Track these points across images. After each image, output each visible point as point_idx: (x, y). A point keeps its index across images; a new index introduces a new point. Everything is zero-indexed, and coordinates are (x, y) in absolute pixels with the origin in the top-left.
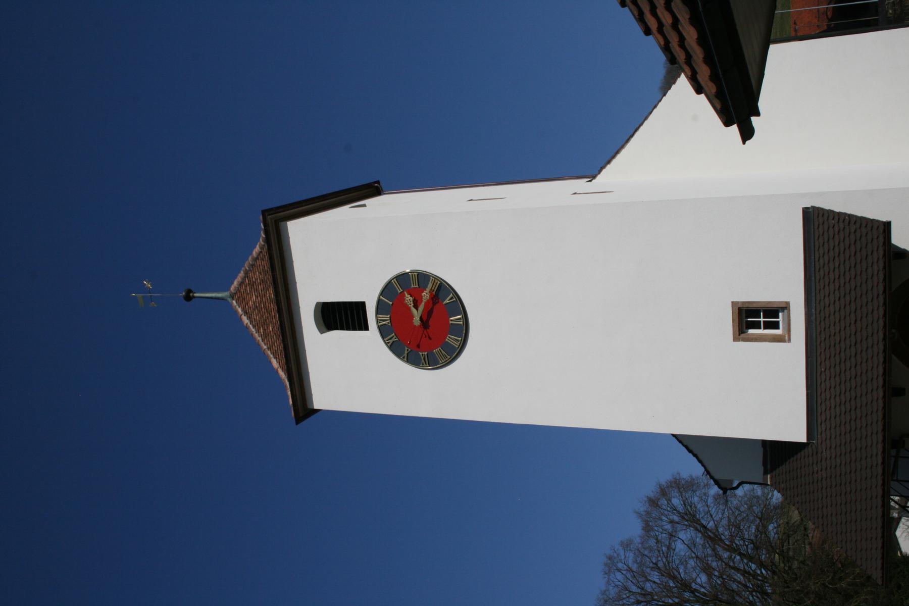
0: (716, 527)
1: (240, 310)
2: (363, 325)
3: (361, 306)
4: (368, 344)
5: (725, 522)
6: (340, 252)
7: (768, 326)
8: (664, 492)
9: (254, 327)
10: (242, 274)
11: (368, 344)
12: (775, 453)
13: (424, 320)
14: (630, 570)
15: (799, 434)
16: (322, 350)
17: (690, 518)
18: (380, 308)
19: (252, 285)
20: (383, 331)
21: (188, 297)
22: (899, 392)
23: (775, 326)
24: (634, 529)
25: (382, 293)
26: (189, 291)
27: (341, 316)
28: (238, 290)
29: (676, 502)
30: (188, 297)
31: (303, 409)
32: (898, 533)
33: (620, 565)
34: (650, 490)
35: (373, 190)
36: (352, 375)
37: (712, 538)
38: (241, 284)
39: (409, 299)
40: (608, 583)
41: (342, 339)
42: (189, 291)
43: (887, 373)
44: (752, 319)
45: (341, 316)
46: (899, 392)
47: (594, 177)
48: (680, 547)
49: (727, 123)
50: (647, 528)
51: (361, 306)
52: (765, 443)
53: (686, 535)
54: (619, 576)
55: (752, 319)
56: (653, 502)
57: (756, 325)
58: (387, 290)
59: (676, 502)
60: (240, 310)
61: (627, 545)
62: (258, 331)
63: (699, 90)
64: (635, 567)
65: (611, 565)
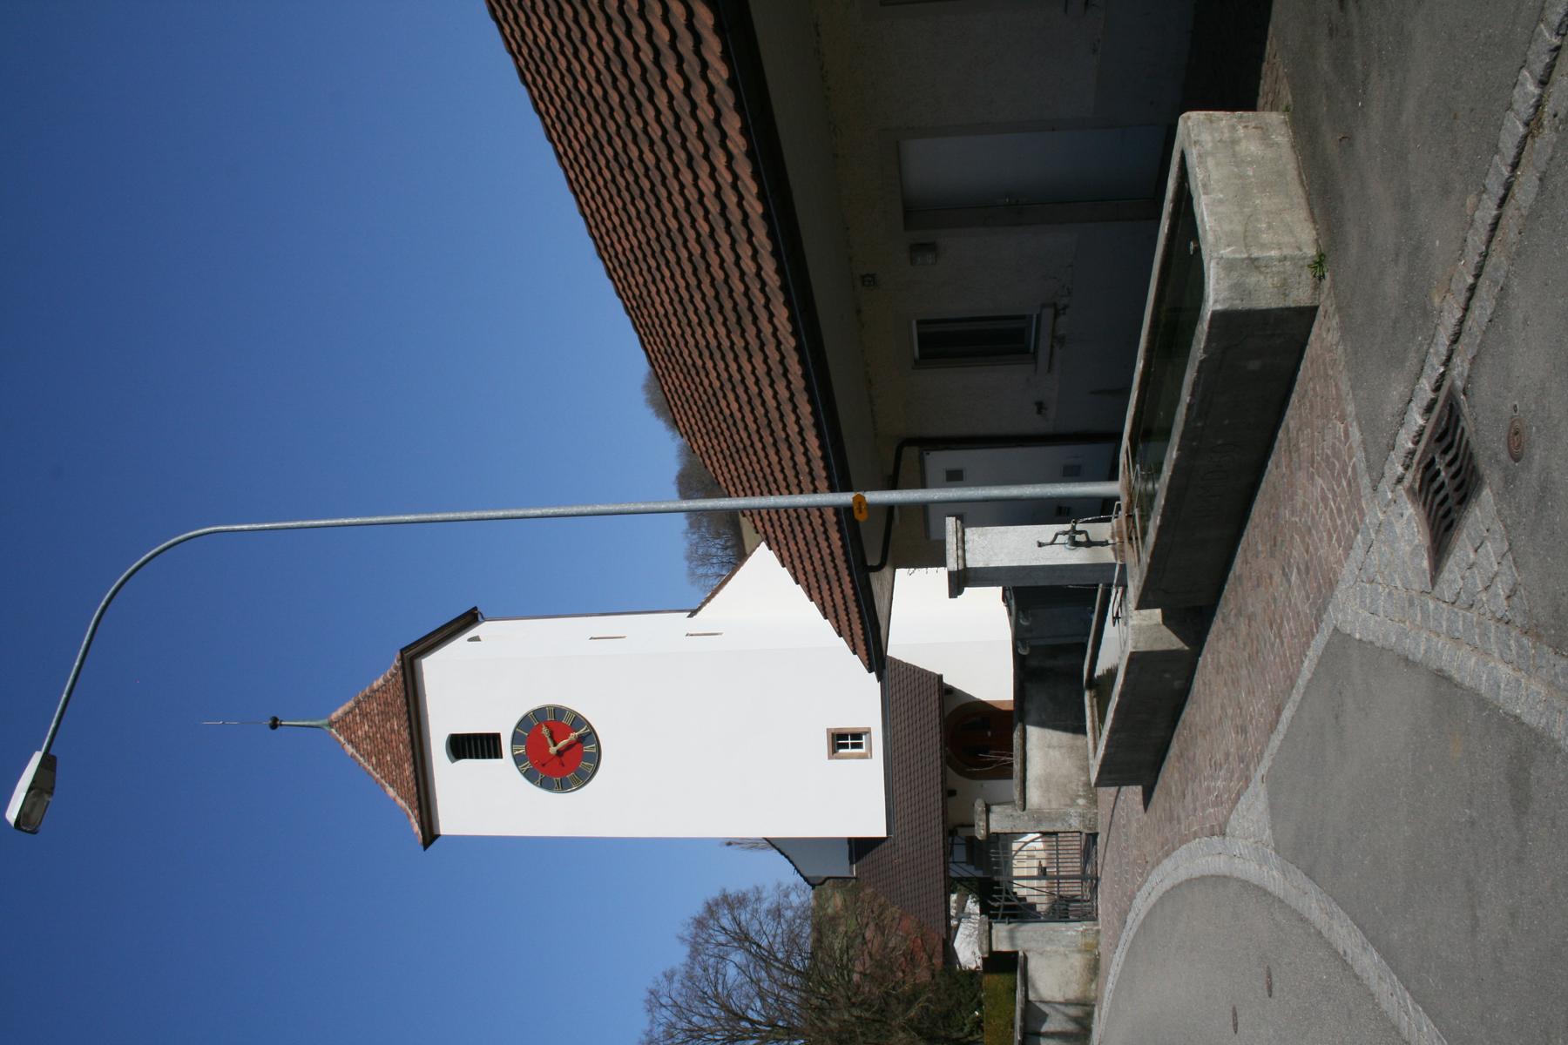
0: (770, 945)
1: (342, 739)
2: (497, 754)
3: (495, 738)
4: (503, 770)
5: (779, 939)
6: (474, 683)
7: (855, 746)
8: (711, 909)
9: (368, 756)
10: (351, 703)
11: (503, 770)
12: (860, 848)
13: (558, 749)
14: (675, 1004)
15: (880, 831)
16: (448, 775)
17: (742, 938)
18: (516, 738)
19: (364, 715)
20: (518, 760)
21: (275, 724)
22: (952, 793)
23: (859, 746)
24: (679, 956)
25: (519, 725)
26: (275, 720)
27: (469, 746)
28: (342, 719)
29: (726, 922)
30: (275, 724)
31: (430, 835)
32: (956, 945)
33: (664, 1000)
34: (698, 909)
35: (470, 619)
36: (482, 801)
37: (765, 958)
38: (347, 714)
39: (545, 731)
40: (652, 1022)
41: (471, 766)
42: (275, 720)
43: (943, 782)
44: (843, 741)
45: (469, 746)
46: (952, 793)
47: (693, 613)
48: (732, 972)
49: (870, 671)
50: (695, 952)
51: (495, 738)
52: (850, 840)
53: (738, 957)
54: (666, 1013)
55: (843, 741)
56: (700, 923)
57: (845, 746)
58: (524, 723)
59: (726, 922)
60: (342, 739)
61: (669, 977)
62: (369, 761)
63: (855, 652)
64: (679, 1000)
65: (654, 1001)
